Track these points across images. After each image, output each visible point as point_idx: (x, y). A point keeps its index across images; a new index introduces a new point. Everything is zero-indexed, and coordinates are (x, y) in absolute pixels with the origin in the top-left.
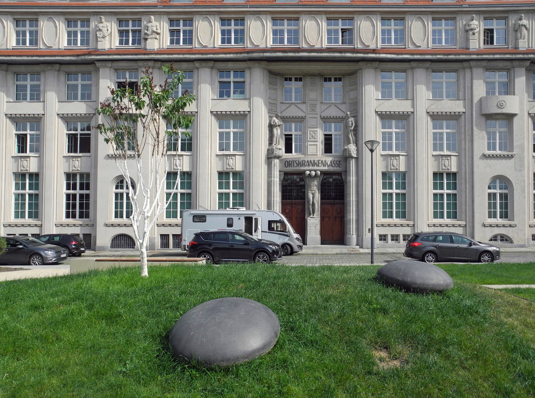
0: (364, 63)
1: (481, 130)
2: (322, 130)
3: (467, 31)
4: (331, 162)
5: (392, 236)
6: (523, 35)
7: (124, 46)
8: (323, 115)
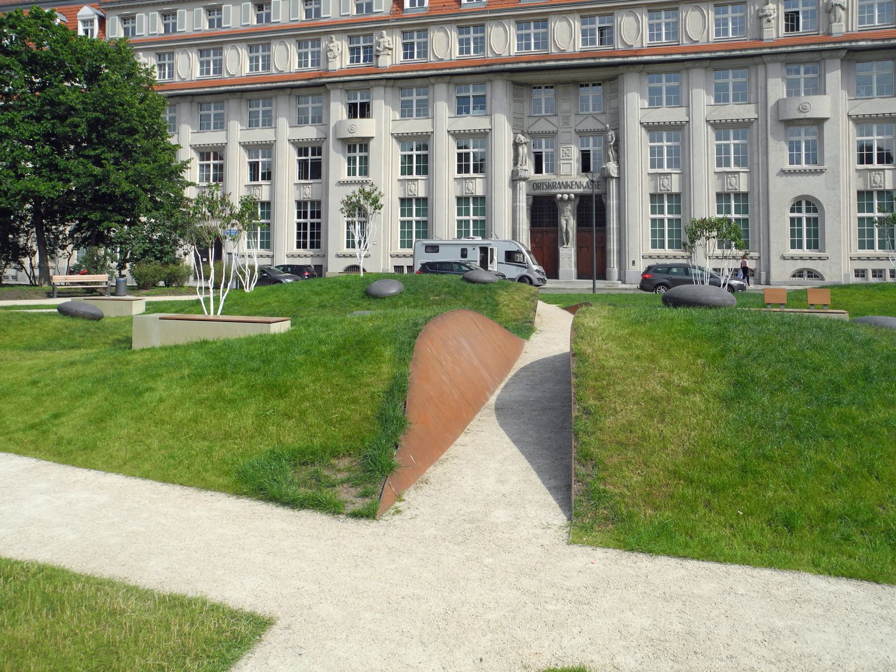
0: (625, 68)
1: (779, 140)
2: (577, 146)
3: (761, 18)
4: (587, 183)
5: (874, 271)
6: (838, 17)
7: (355, 64)
8: (578, 128)
